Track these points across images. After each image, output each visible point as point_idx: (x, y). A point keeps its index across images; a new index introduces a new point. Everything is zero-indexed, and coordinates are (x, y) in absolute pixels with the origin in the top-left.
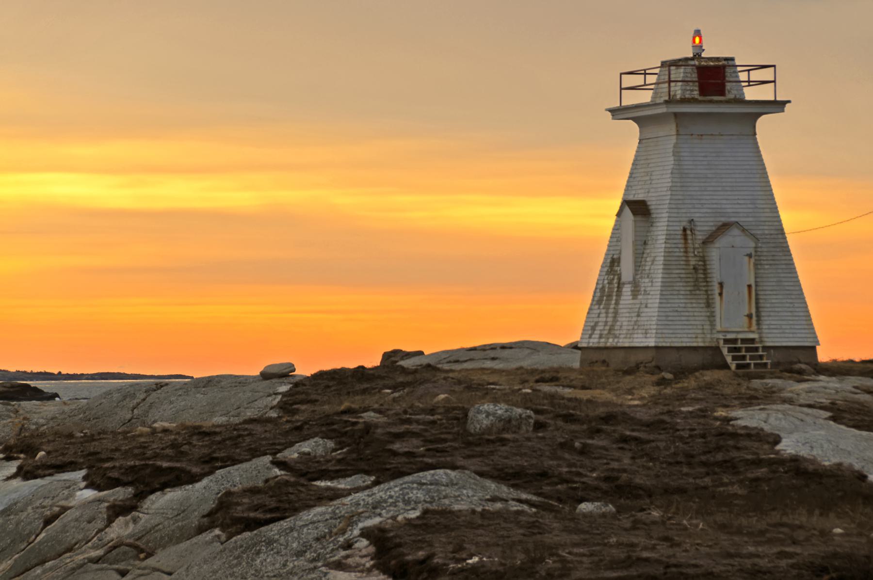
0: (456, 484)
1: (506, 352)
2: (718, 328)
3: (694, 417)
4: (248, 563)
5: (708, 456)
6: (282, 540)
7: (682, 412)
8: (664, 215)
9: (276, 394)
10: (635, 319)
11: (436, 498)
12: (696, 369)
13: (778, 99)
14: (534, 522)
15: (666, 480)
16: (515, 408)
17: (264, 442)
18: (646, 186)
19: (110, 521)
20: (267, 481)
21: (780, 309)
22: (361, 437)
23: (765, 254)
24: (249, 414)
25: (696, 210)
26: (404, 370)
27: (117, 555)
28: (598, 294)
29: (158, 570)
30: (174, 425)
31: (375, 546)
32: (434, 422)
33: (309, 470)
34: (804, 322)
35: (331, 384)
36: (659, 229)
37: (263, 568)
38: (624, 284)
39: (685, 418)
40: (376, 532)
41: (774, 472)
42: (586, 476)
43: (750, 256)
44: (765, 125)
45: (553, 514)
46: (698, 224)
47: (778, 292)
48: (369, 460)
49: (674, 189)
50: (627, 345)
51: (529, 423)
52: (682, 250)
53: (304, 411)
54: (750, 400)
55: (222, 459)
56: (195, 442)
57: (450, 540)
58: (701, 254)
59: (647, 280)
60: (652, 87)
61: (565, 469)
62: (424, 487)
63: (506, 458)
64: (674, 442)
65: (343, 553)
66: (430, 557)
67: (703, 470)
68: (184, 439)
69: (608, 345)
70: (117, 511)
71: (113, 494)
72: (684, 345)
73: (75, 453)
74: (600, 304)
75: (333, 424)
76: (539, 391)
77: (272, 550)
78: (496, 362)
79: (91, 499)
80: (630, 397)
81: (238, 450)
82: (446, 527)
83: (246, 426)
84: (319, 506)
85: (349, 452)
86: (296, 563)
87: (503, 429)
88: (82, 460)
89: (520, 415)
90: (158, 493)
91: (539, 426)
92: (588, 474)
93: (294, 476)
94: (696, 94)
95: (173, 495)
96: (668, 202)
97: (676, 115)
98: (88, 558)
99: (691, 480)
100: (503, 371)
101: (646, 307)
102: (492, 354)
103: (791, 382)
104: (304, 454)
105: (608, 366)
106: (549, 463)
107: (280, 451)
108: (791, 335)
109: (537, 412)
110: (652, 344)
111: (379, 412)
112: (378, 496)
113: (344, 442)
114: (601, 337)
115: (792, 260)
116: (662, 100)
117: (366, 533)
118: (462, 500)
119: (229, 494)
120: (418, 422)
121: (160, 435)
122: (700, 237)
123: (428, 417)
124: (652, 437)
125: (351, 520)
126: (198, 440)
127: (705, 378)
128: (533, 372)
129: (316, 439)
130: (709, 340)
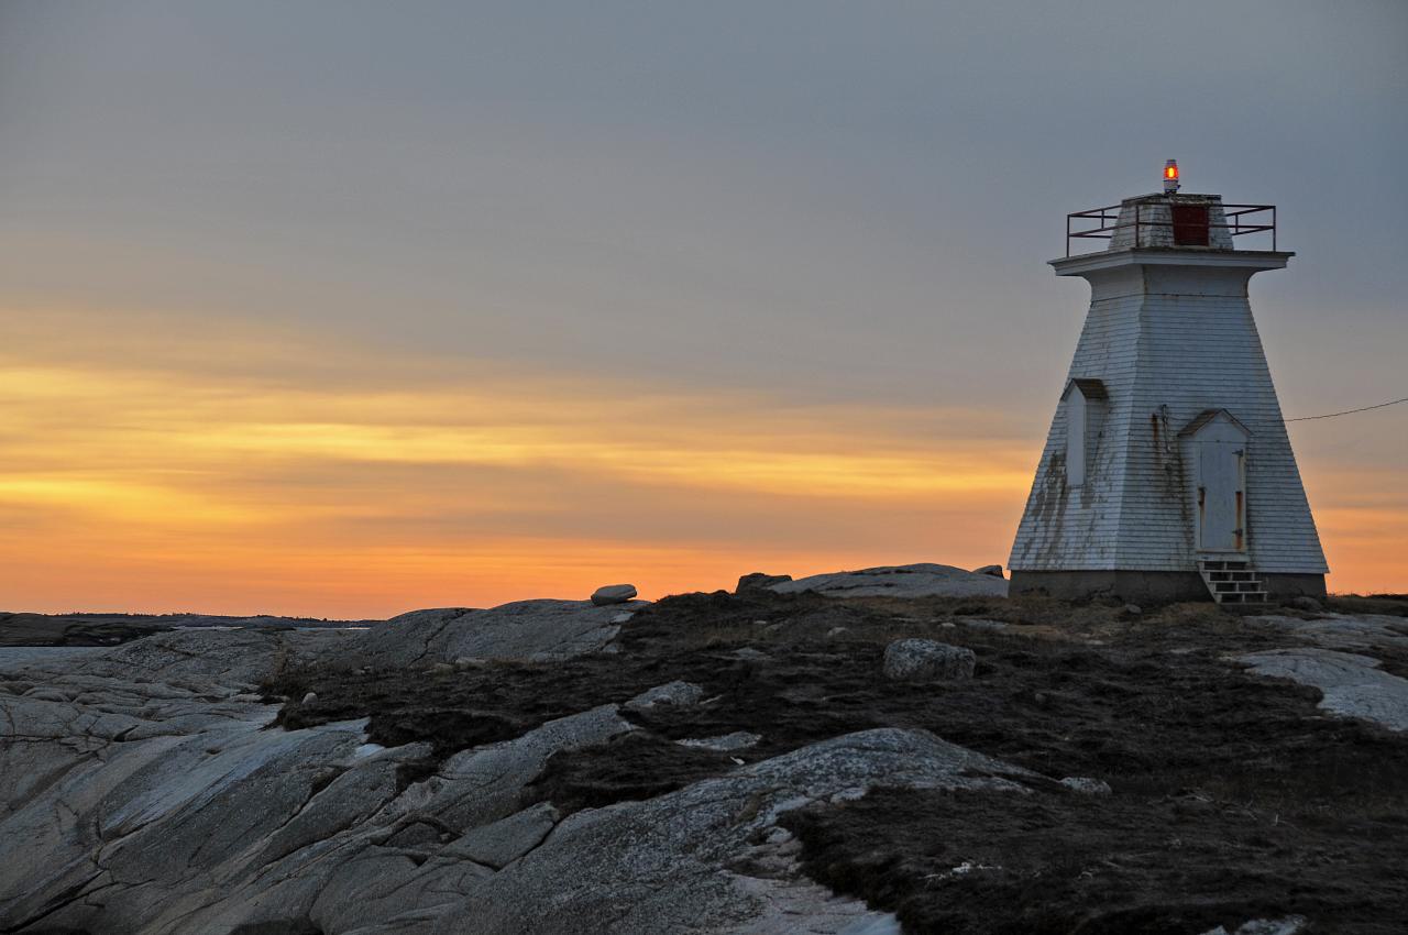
0: (913, 750)
1: (904, 577)
2: (1198, 547)
3: (1192, 663)
4: (610, 860)
5: (1223, 715)
6: (661, 827)
7: (1174, 656)
8: (1127, 399)
9: (613, 624)
10: (1086, 534)
11: (887, 770)
12: (1169, 602)
13: (1277, 250)
14: (1034, 809)
15: (1168, 748)
16: (948, 646)
17: (607, 686)
18: (1103, 361)
19: (400, 789)
20: (613, 738)
21: (1277, 525)
22: (738, 681)
23: (1258, 452)
24: (578, 649)
25: (1170, 393)
26: (777, 597)
27: (411, 834)
28: (1035, 502)
29: (468, 858)
30: (483, 661)
31: (801, 839)
32: (837, 663)
33: (670, 724)
34: (1308, 543)
35: (685, 612)
36: (1120, 416)
37: (634, 869)
38: (1070, 488)
39: (1180, 663)
40: (802, 819)
41: (1324, 740)
42: (1055, 740)
43: (1240, 454)
44: (1257, 282)
45: (1059, 796)
46: (1173, 410)
47: (1275, 503)
48: (752, 712)
49: (1142, 364)
50: (1075, 568)
51: (969, 666)
52: (1151, 444)
53: (652, 647)
54: (1257, 642)
55: (551, 708)
56: (513, 684)
57: (917, 834)
58: (1176, 451)
59: (1104, 483)
60: (1110, 233)
61: (1026, 731)
62: (868, 753)
63: (941, 713)
64: (1172, 696)
65: (753, 849)
66: (894, 861)
67: (1217, 735)
68: (498, 679)
69: (1049, 567)
70: (412, 774)
71: (405, 752)
72: (1153, 568)
73: (355, 695)
74: (1038, 515)
75: (700, 663)
76: (964, 625)
77: (646, 841)
78: (892, 589)
79: (376, 756)
80: (1087, 635)
81: (572, 696)
82: (906, 814)
83: (581, 664)
84: (711, 777)
85: (723, 701)
86: (683, 863)
87: (935, 675)
88: (363, 705)
89: (957, 655)
90: (466, 751)
91: (982, 671)
92: (1059, 737)
93: (650, 732)
94: (1170, 242)
95: (484, 755)
96: (1133, 381)
97: (1144, 267)
98: (371, 838)
99: (1203, 749)
100: (910, 600)
101: (1103, 518)
102: (886, 579)
103: (1297, 619)
104: (662, 702)
105: (1048, 595)
106: (1002, 721)
107: (629, 698)
108: (1291, 559)
109: (978, 652)
110: (1112, 567)
111: (760, 648)
112: (800, 765)
113: (715, 687)
114: (1038, 557)
115: (1294, 460)
116: (1127, 248)
117: (785, 820)
118: (925, 773)
119: (562, 754)
120: (816, 662)
121: (465, 674)
122: (1175, 428)
123: (827, 655)
124: (1137, 688)
125: (762, 799)
126: (517, 681)
127: (1184, 612)
128: (951, 600)
129: (677, 683)
130: (1185, 563)
